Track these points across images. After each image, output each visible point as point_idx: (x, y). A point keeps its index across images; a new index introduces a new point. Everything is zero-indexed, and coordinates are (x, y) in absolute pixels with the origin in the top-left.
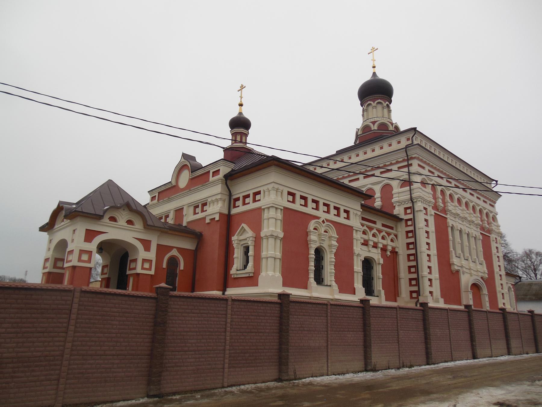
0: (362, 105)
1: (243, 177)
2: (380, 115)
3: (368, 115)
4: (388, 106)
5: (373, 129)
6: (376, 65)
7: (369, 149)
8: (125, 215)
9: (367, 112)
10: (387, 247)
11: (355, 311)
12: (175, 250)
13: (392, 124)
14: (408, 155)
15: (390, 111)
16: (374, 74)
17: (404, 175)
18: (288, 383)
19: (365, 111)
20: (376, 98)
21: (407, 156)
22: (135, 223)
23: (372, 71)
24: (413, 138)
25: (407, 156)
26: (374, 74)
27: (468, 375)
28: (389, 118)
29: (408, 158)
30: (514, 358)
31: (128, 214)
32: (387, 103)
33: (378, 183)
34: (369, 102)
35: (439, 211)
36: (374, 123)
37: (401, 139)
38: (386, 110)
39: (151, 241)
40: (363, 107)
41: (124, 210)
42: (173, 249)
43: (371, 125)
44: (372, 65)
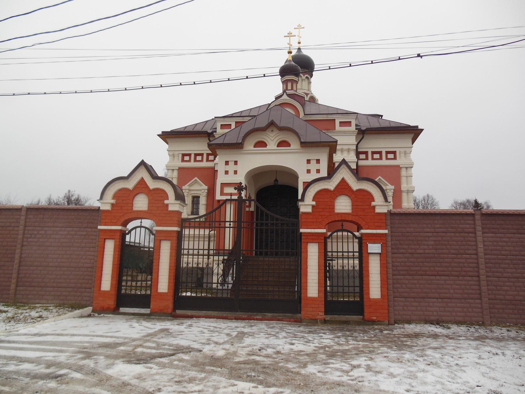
1: (11, 208)
8: (274, 137)
11: (448, 225)
12: (344, 167)
18: (236, 359)
22: (291, 144)
24: (126, 175)
30: (196, 374)
31: (278, 135)
41: (272, 131)
42: (207, 209)
44: (298, 41)
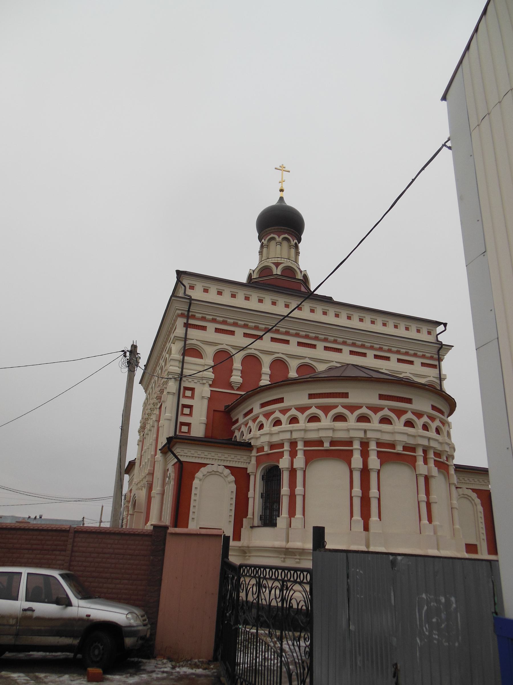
0: (260, 239)
2: (285, 255)
3: (268, 253)
4: (296, 247)
5: (275, 273)
6: (284, 188)
7: (268, 298)
9: (267, 248)
10: (273, 443)
13: (301, 272)
14: (190, 310)
15: (297, 253)
16: (281, 199)
17: (430, 376)
19: (266, 246)
20: (282, 230)
21: (189, 311)
23: (280, 194)
25: (189, 311)
26: (281, 199)
27: (249, 621)
28: (296, 261)
29: (188, 313)
32: (296, 241)
33: (396, 372)
34: (272, 235)
35: (235, 390)
36: (277, 265)
37: (251, 295)
38: (293, 251)
39: (348, 393)
40: (263, 241)
43: (274, 267)
44: (279, 188)
